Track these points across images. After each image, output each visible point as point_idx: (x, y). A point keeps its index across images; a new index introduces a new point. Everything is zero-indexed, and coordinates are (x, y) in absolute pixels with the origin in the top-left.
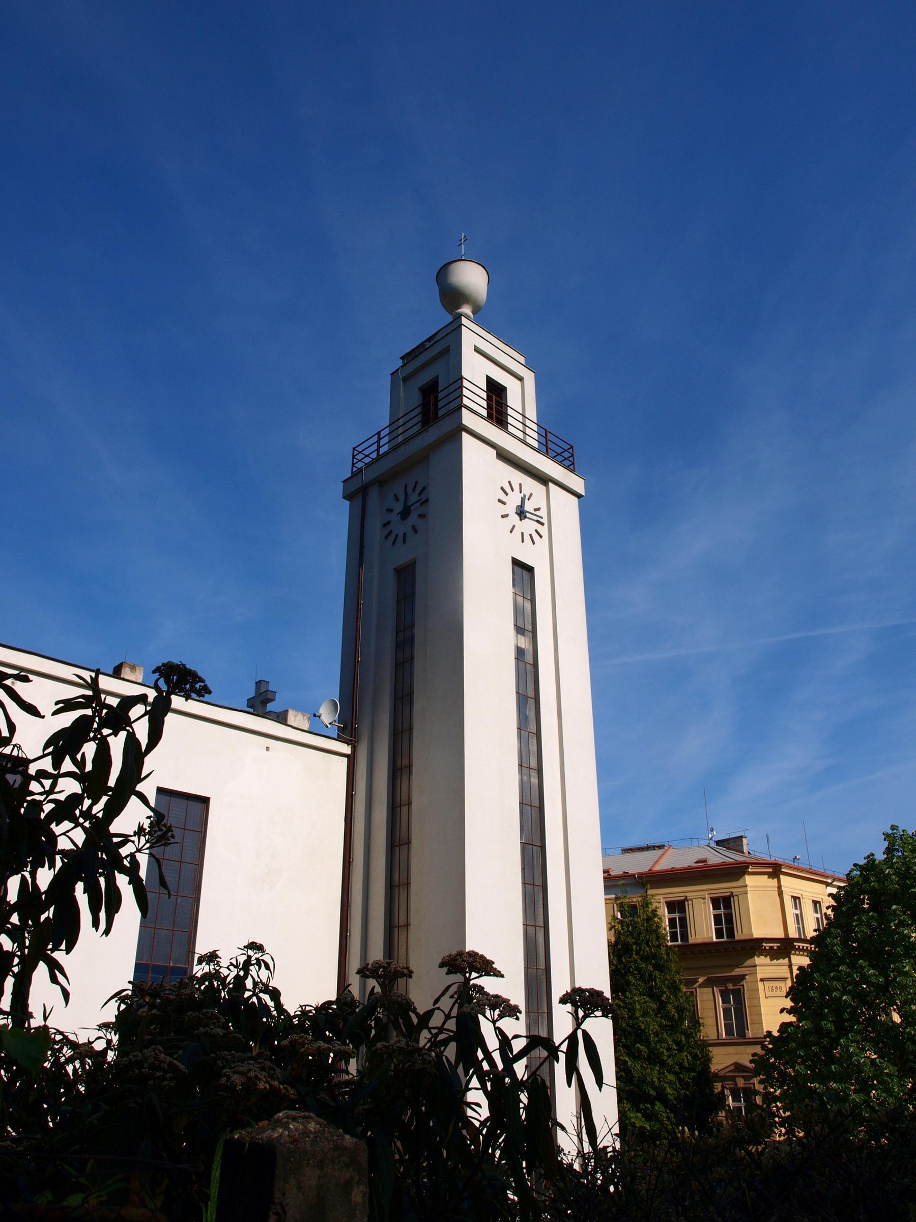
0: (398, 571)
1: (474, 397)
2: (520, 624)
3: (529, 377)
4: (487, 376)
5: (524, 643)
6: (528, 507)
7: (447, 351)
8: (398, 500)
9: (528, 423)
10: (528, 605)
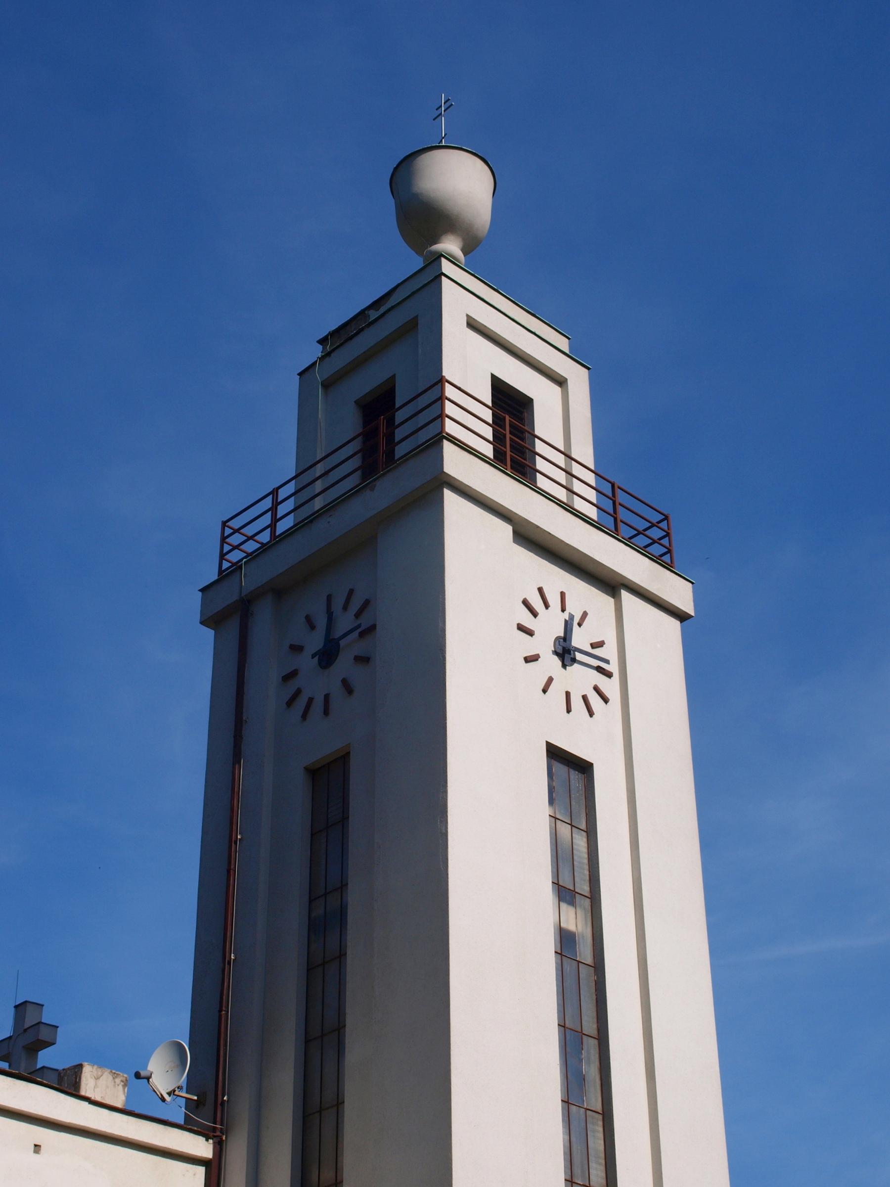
0: (314, 773)
1: (468, 419)
2: (566, 881)
3: (578, 378)
4: (493, 376)
5: (574, 920)
6: (580, 639)
7: (412, 326)
8: (312, 627)
9: (576, 470)
10: (581, 842)
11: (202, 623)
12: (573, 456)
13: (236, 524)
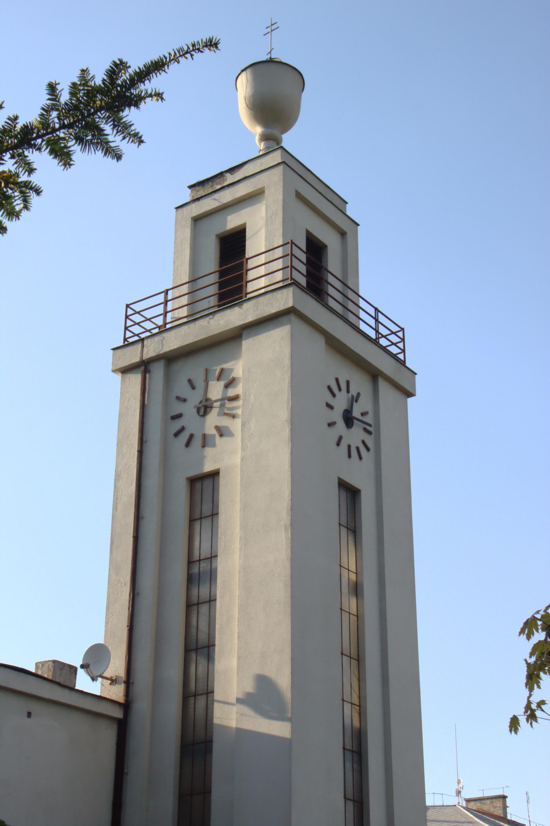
0: (193, 481)
5: (352, 604)
6: (356, 413)
11: (113, 371)
12: (350, 285)
13: (137, 307)
